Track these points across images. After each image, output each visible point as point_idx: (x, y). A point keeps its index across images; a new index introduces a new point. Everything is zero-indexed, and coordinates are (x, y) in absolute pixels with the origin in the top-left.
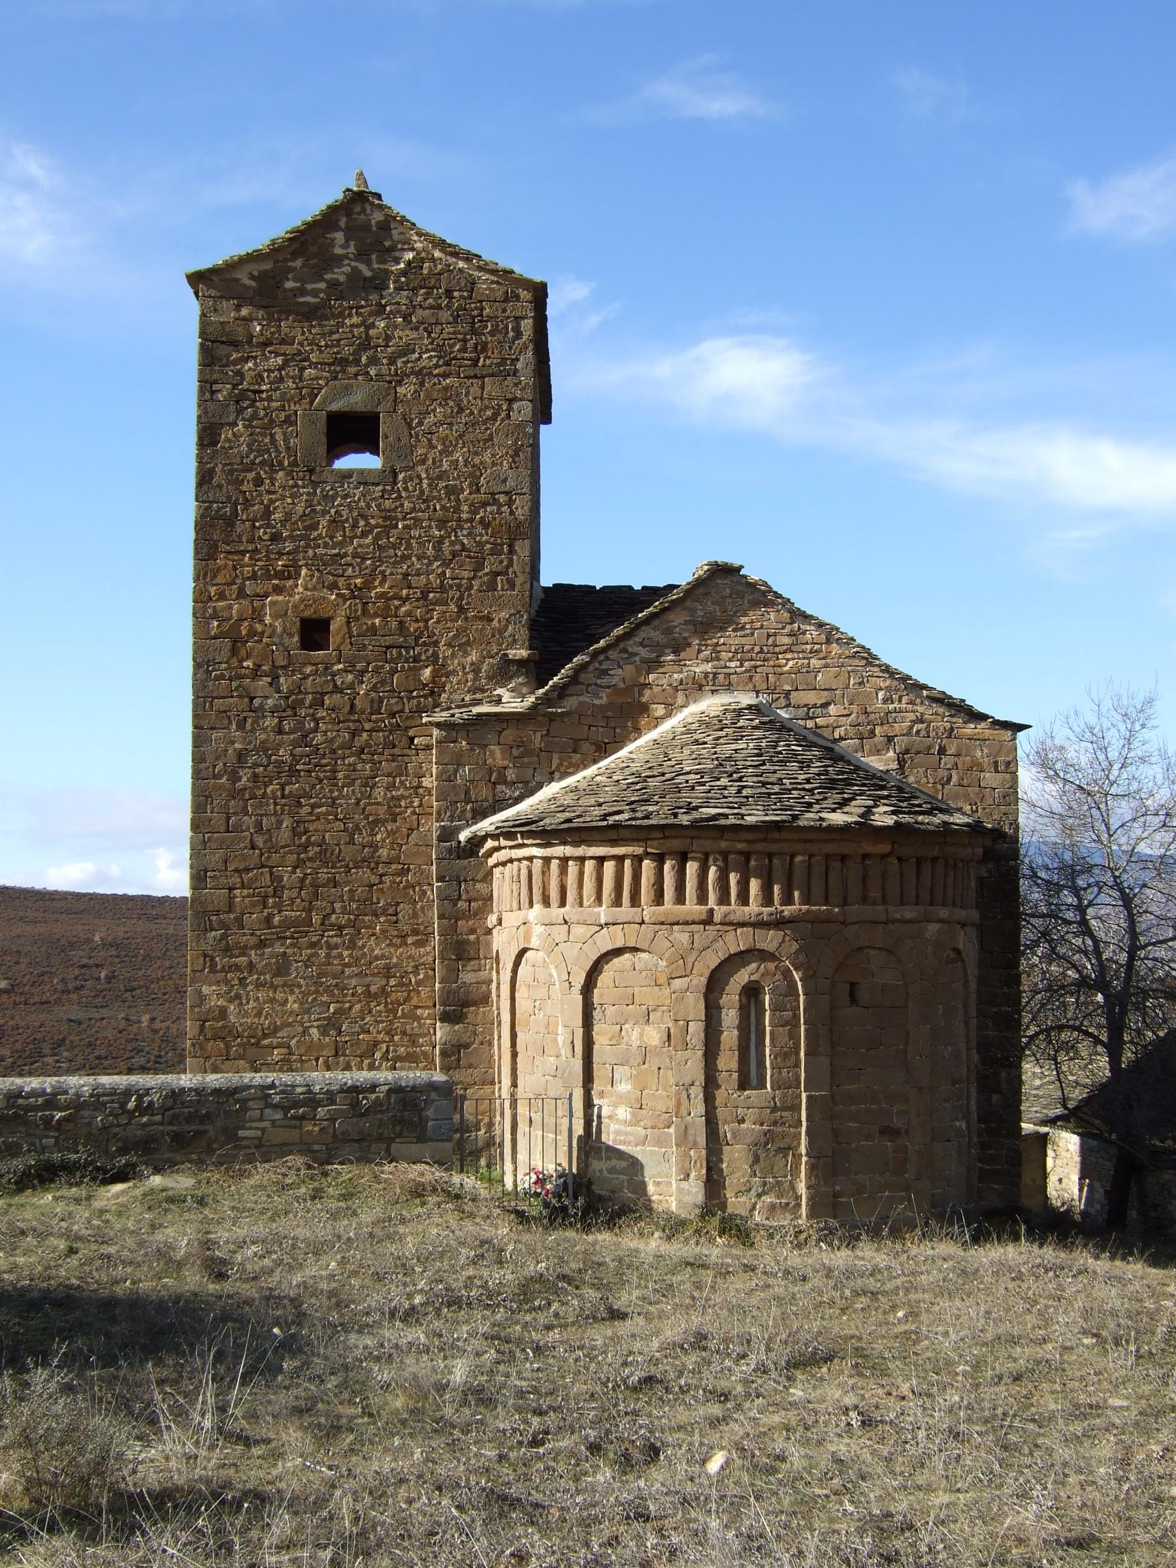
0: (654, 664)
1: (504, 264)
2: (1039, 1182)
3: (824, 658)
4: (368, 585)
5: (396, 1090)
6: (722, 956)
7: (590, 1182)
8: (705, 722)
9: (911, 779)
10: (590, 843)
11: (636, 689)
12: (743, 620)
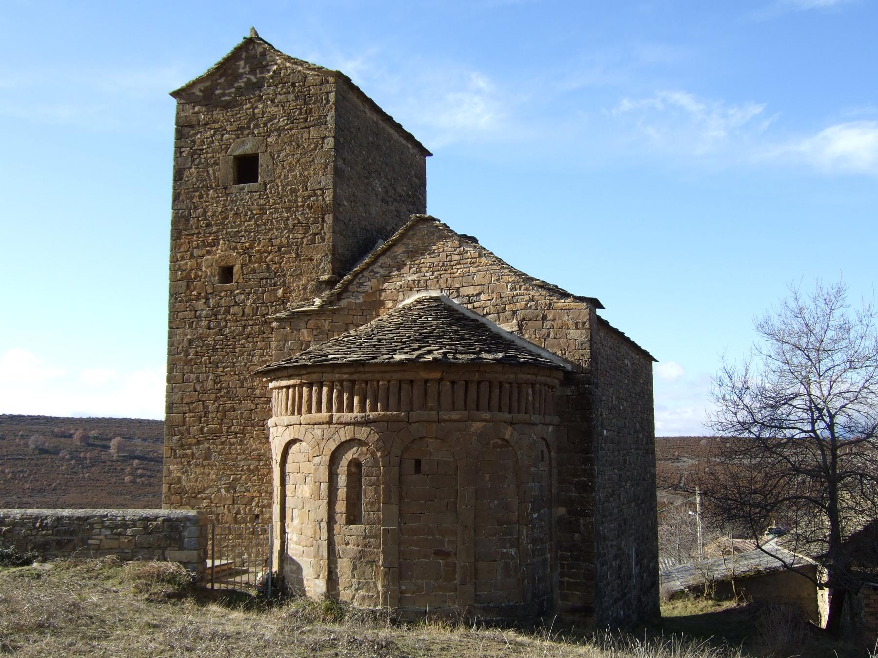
0: (387, 278)
1: (319, 64)
2: (813, 596)
4: (252, 247)
5: (168, 520)
9: (526, 336)
12: (434, 247)
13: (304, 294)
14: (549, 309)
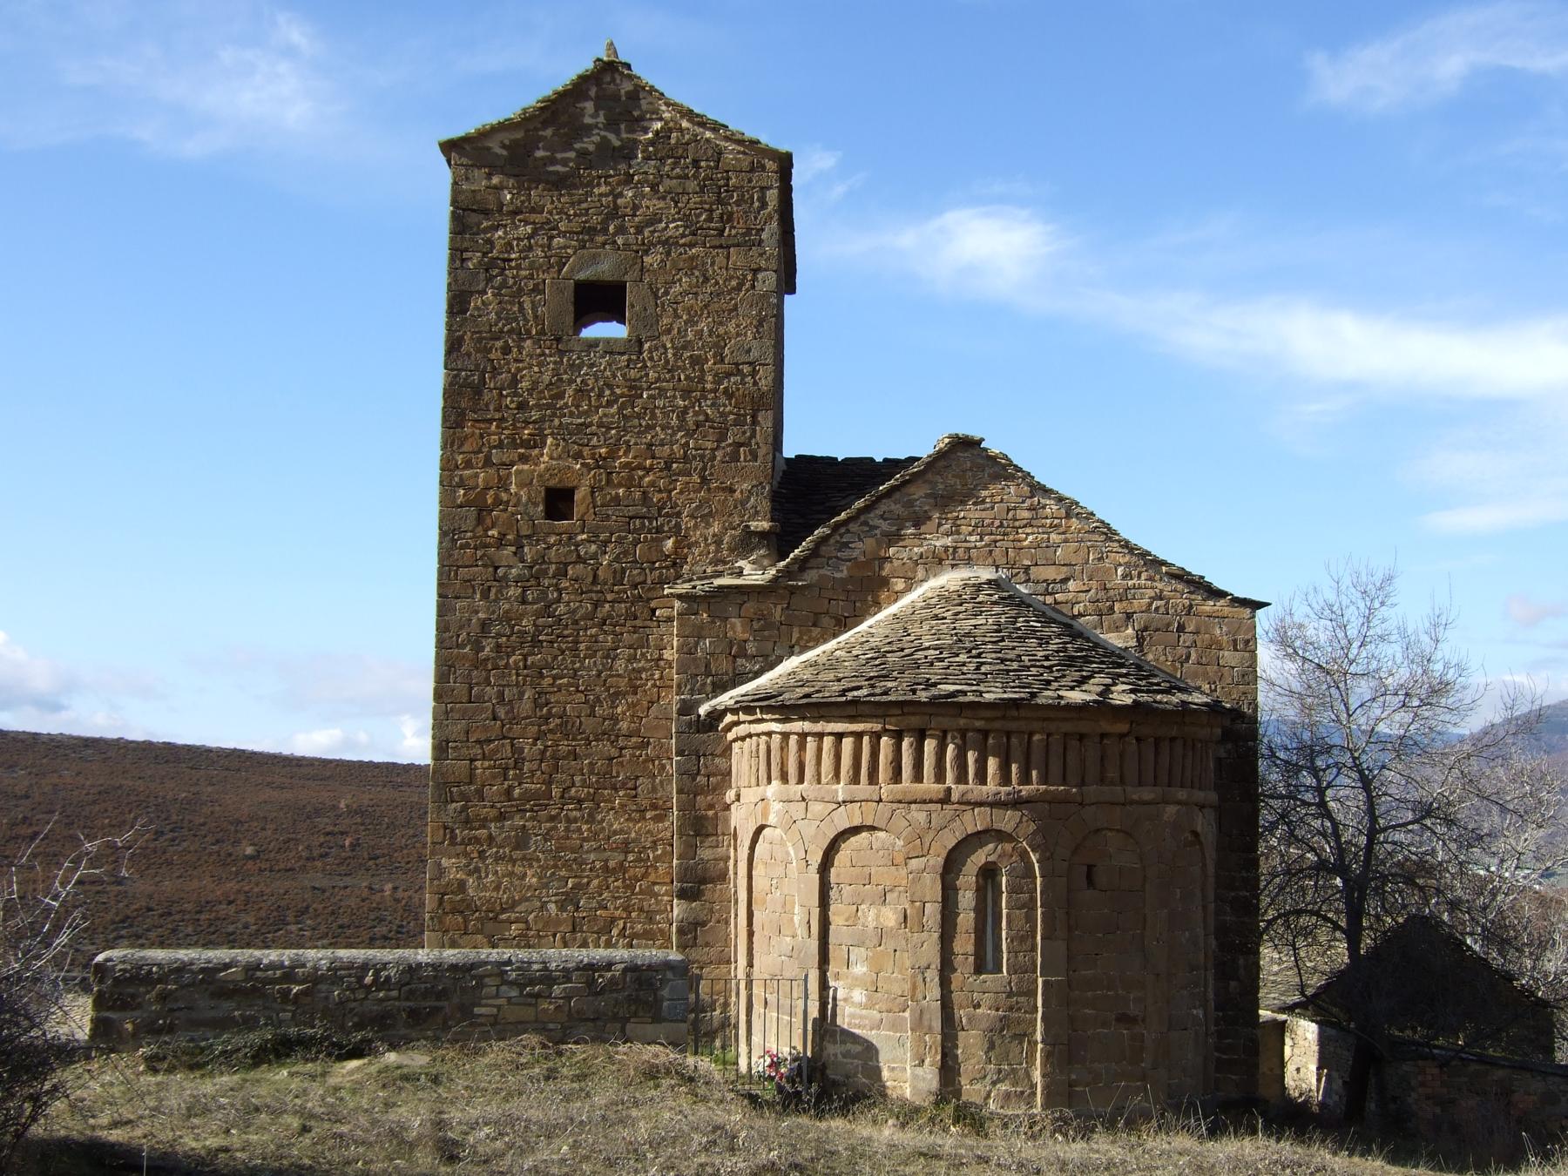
0: (894, 538)
1: (750, 134)
4: (612, 455)
5: (632, 968)
6: (959, 836)
7: (824, 1067)
8: (945, 597)
9: (1150, 657)
12: (984, 493)
13: (717, 551)
14: (1188, 614)
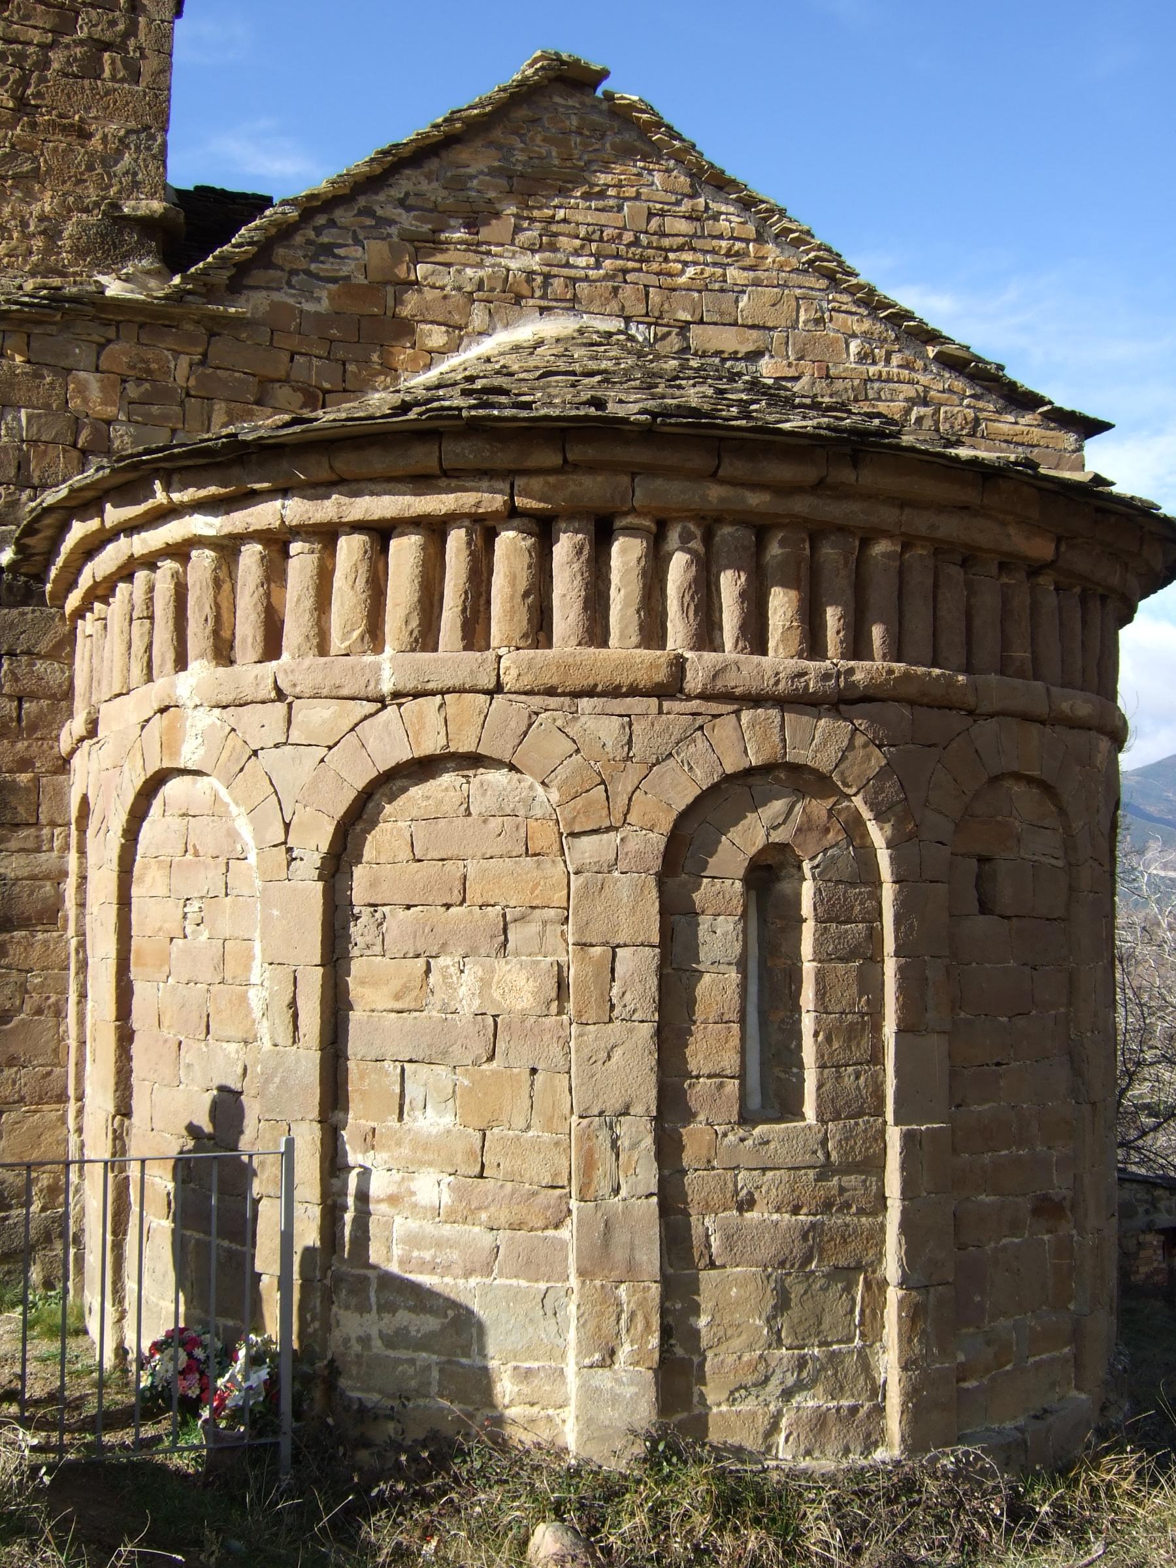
0: (426, 245)
3: (752, 268)
6: (704, 778)
7: (334, 1370)
10: (352, 485)
11: (390, 289)
12: (603, 179)
13: (47, 251)
